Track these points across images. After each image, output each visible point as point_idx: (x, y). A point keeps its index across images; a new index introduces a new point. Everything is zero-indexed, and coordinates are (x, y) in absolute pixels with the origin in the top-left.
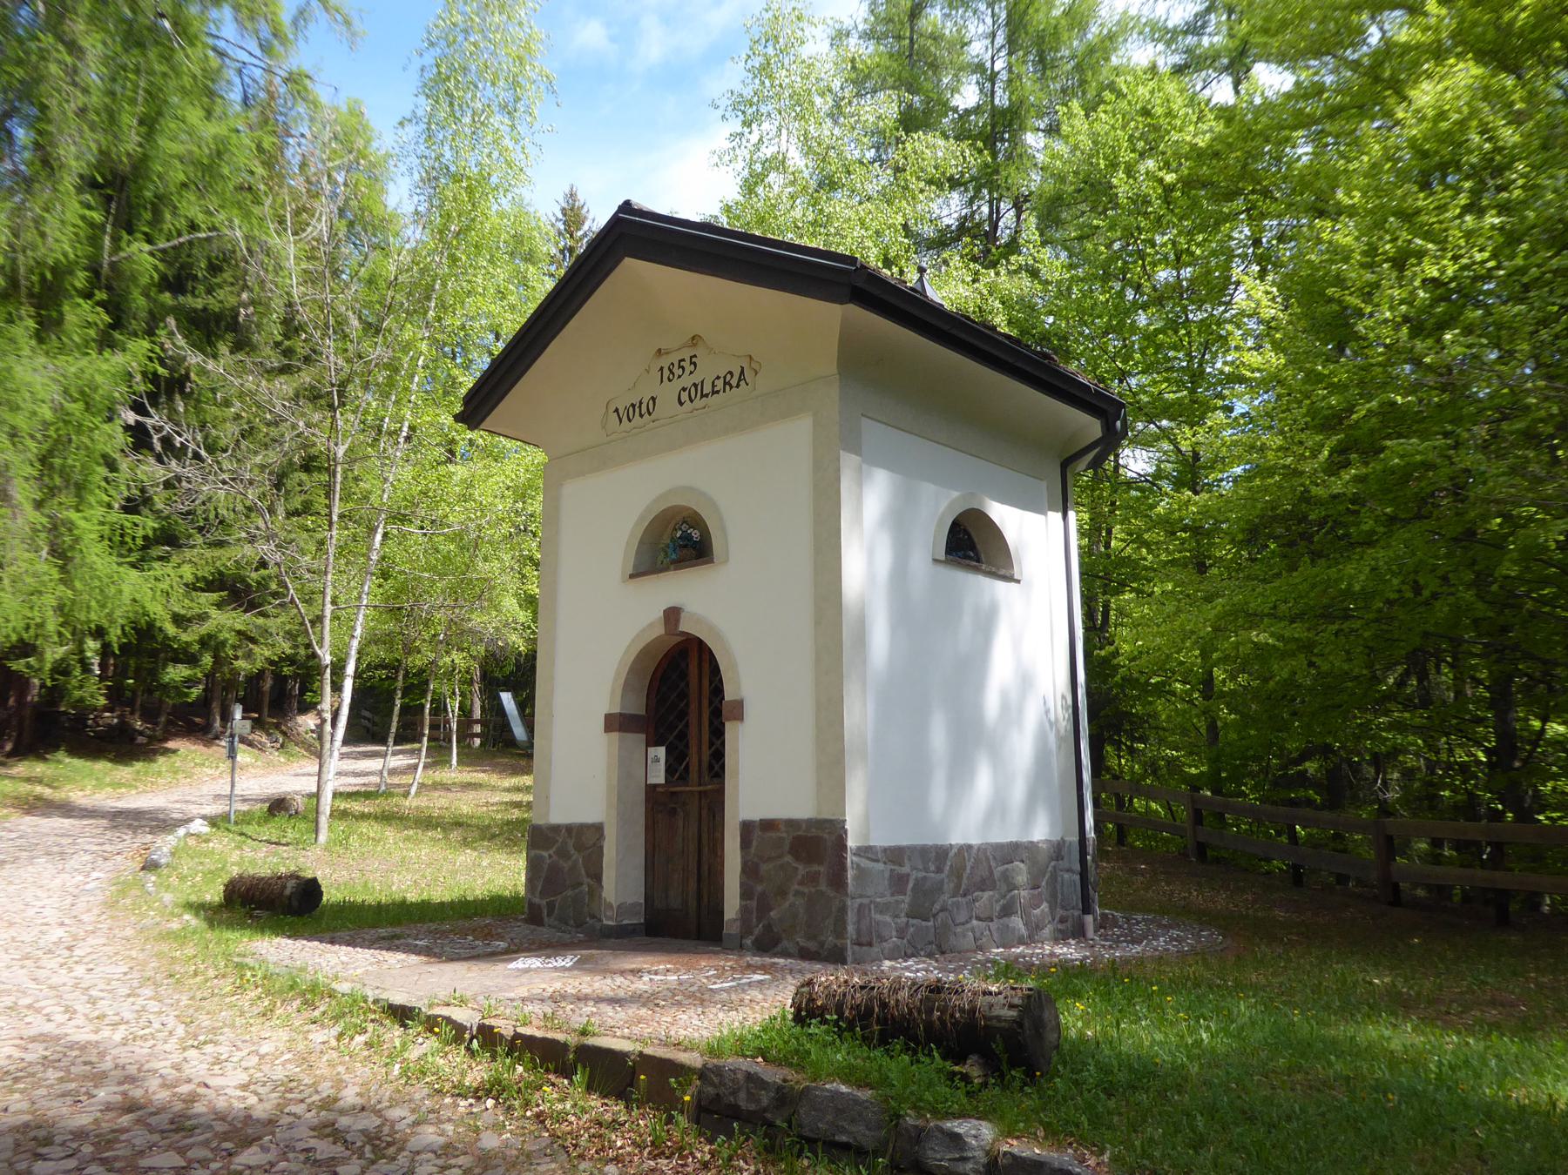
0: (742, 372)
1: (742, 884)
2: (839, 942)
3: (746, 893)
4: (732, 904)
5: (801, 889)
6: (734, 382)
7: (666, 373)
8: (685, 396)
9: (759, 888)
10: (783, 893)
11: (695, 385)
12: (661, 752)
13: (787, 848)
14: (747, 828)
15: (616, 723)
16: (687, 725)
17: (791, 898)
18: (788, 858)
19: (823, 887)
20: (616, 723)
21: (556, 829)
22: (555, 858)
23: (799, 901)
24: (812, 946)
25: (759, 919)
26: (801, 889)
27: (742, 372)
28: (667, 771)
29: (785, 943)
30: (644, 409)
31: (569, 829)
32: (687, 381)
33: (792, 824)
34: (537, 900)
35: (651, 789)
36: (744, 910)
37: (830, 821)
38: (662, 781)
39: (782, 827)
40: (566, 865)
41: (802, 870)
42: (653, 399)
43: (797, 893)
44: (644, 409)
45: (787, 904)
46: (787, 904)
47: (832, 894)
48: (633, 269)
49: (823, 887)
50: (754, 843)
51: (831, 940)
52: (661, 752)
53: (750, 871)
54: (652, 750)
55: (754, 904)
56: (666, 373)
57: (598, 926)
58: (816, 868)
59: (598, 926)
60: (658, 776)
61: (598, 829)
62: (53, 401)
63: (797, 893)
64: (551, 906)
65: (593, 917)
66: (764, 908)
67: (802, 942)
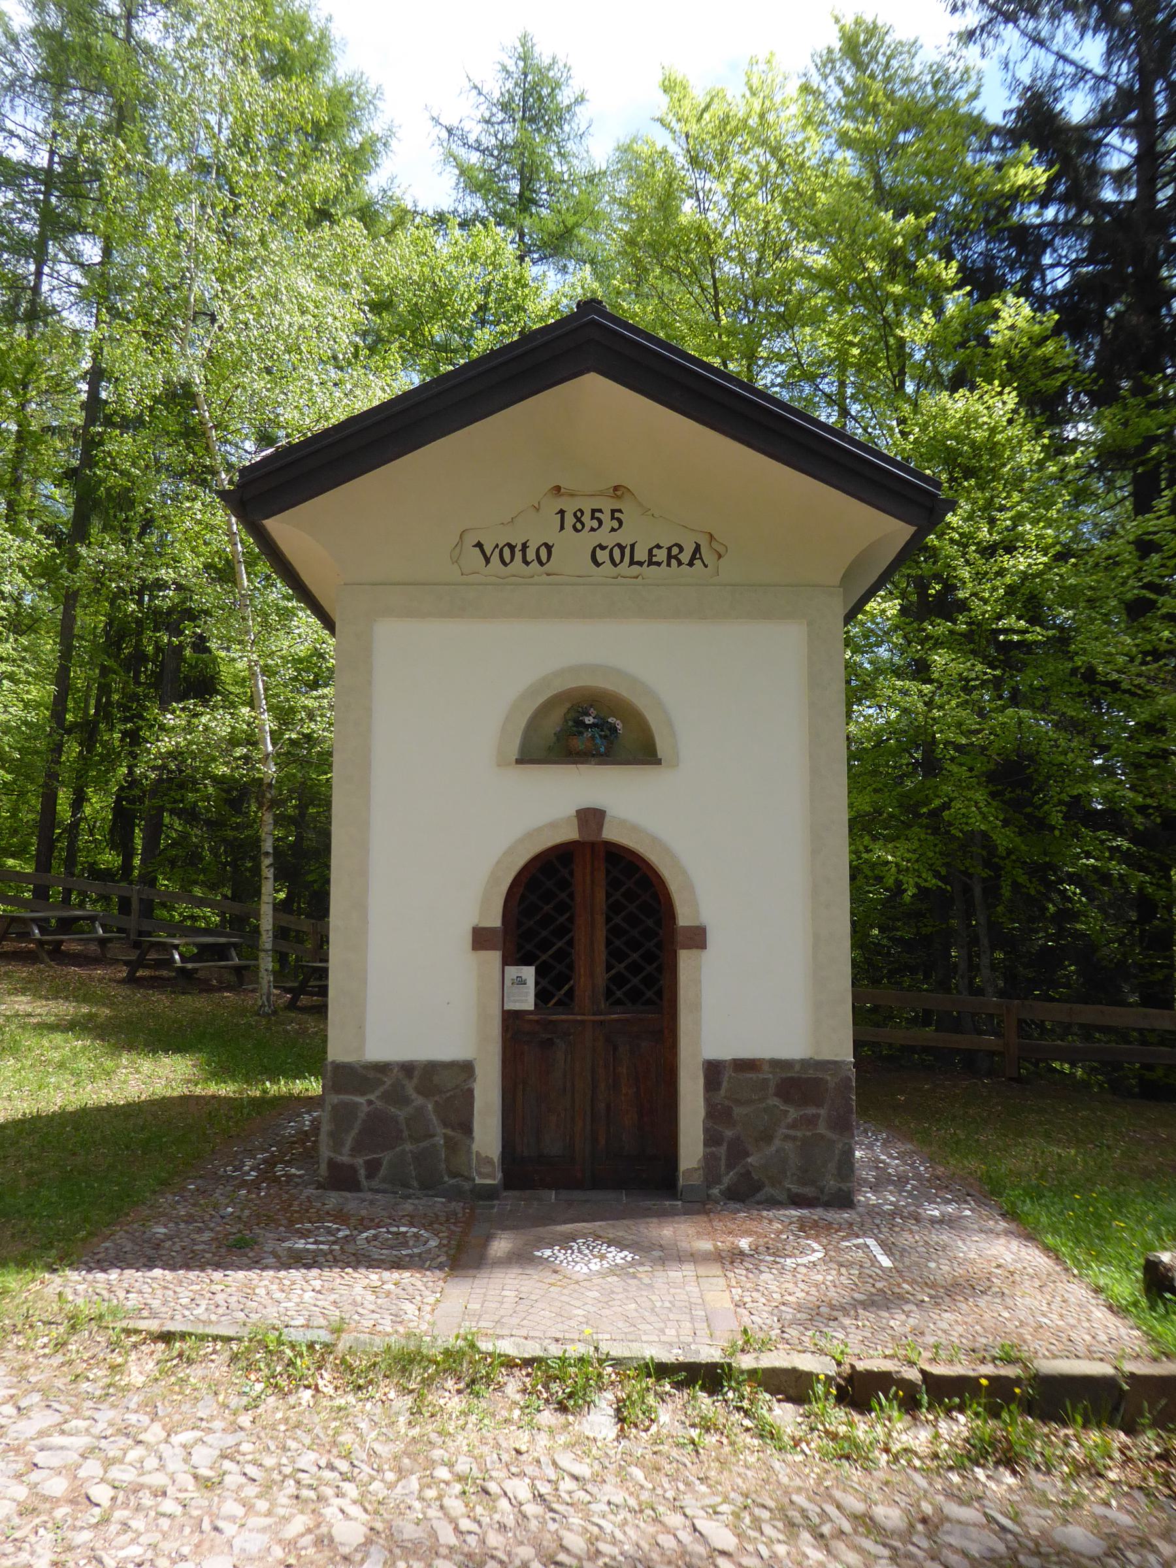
0: (698, 548)
1: (706, 1130)
2: (844, 1186)
3: (712, 1139)
4: (691, 1147)
5: (792, 1132)
6: (685, 557)
7: (570, 520)
8: (602, 556)
9: (729, 1133)
10: (766, 1137)
11: (622, 548)
12: (529, 973)
13: (771, 1090)
14: (713, 1071)
15: (481, 939)
16: (571, 943)
17: (777, 1143)
18: (774, 1101)
19: (822, 1129)
20: (481, 939)
21: (382, 1068)
22: (379, 1104)
23: (789, 1146)
24: (809, 1191)
25: (730, 1167)
26: (792, 1132)
27: (698, 548)
28: (537, 996)
29: (768, 1190)
30: (531, 555)
31: (408, 1068)
32: (604, 536)
33: (776, 1064)
34: (344, 1158)
35: (511, 1018)
36: (709, 1161)
37: (835, 1063)
38: (532, 1008)
39: (766, 1067)
40: (401, 1114)
41: (793, 1113)
42: (549, 548)
43: (787, 1137)
44: (531, 555)
45: (773, 1148)
46: (773, 1148)
47: (834, 1137)
48: (596, 394)
49: (822, 1129)
50: (725, 1085)
51: (831, 1184)
52: (529, 973)
53: (716, 1114)
54: (512, 971)
55: (722, 1150)
56: (570, 520)
57: (467, 1186)
58: (811, 1111)
59: (467, 1186)
60: (525, 1000)
61: (466, 1069)
62: (89, 545)
63: (787, 1137)
64: (373, 1168)
65: (454, 1175)
66: (737, 1152)
67: (795, 1188)
